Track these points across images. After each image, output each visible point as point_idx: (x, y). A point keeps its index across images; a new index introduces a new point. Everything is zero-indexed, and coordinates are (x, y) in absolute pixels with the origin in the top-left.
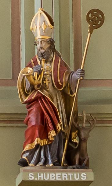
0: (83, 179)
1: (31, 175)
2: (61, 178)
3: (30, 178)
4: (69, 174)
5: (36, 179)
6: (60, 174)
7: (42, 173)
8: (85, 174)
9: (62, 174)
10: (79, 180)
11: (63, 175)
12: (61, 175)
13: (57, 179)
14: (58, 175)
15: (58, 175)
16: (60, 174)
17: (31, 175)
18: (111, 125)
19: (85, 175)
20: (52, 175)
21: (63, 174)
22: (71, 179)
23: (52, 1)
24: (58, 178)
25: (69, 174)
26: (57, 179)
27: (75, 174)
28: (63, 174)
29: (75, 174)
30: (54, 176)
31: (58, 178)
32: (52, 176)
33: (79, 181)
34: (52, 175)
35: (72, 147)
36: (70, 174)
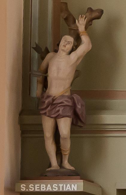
0: (54, 190)
1: (23, 186)
2: (40, 189)
3: (22, 190)
4: (59, 185)
5: (27, 190)
6: (39, 185)
7: (65, 184)
8: (57, 185)
9: (40, 185)
10: (58, 191)
11: (42, 186)
12: (40, 186)
13: (41, 190)
14: (37, 186)
15: (37, 186)
16: (39, 185)
17: (23, 186)
18: (125, 135)
19: (56, 186)
20: (43, 186)
21: (42, 185)
22: (61, 190)
23: (31, 1)
24: (38, 189)
25: (59, 185)
26: (36, 190)
27: (65, 185)
28: (42, 185)
29: (65, 185)
30: (44, 187)
31: (38, 189)
32: (43, 187)
33: (57, 192)
34: (43, 186)
35: (21, 156)
36: (61, 185)
